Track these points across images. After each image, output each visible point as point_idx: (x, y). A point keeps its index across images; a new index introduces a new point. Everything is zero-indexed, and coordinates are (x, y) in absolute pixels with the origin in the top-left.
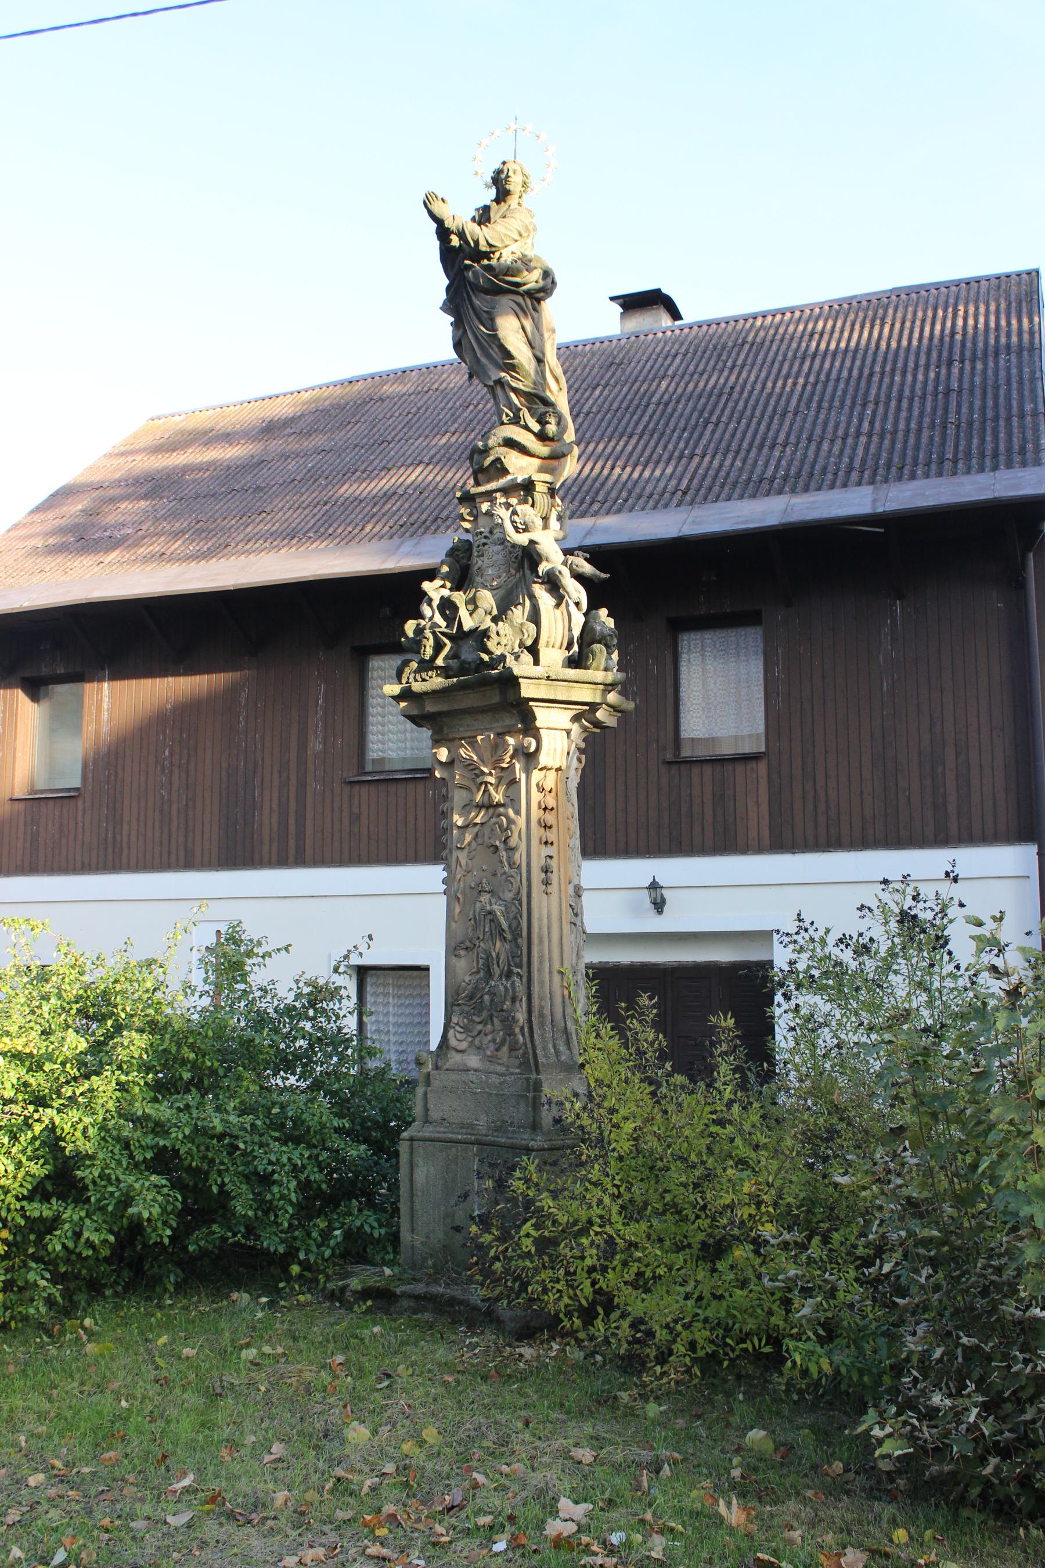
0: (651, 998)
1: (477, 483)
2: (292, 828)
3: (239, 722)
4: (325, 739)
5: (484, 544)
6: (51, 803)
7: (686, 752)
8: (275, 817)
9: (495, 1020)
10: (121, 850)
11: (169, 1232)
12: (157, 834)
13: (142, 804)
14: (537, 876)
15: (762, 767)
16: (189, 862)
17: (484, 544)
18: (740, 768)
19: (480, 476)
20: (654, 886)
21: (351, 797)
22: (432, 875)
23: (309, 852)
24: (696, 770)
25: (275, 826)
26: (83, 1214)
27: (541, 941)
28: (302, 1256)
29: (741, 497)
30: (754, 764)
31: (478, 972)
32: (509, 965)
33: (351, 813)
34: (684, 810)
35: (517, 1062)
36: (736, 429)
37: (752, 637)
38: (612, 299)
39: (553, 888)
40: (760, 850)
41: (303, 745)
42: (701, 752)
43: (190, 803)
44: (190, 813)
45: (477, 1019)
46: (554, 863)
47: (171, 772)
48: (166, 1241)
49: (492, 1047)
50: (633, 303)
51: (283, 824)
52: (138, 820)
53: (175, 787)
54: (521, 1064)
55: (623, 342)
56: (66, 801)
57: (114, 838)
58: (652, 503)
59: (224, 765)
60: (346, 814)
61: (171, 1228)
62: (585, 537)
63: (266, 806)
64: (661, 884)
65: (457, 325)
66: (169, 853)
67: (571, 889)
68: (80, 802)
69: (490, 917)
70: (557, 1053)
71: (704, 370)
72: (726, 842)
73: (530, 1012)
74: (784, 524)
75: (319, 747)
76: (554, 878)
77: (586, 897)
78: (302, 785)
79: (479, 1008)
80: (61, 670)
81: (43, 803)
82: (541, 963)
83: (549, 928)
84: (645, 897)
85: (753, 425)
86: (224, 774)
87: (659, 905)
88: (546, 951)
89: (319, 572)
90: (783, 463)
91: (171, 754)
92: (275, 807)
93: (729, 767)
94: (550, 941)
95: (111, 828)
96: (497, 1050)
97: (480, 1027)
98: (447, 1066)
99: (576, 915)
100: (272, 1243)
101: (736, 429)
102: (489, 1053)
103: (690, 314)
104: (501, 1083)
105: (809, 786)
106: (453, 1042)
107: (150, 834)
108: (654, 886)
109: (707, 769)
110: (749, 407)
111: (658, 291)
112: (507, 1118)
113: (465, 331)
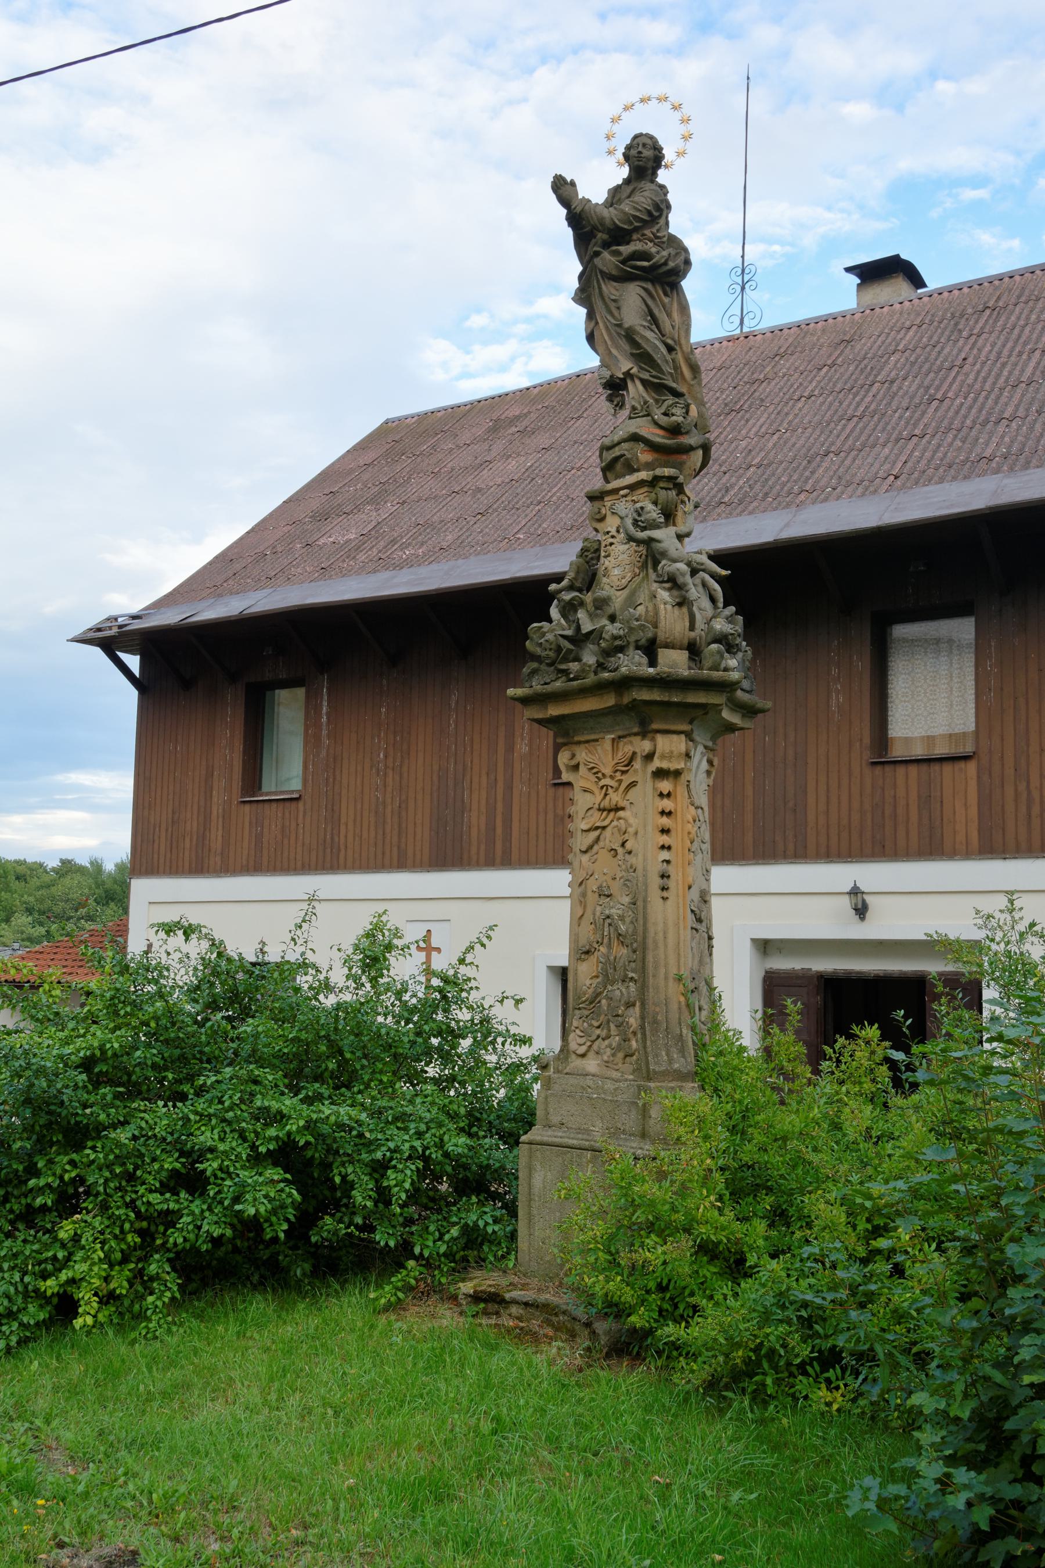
0: (795, 1003)
1: (607, 481)
2: (499, 831)
3: (449, 725)
4: (531, 740)
5: (611, 544)
6: (274, 805)
7: (898, 752)
8: (483, 818)
9: (612, 1025)
10: (339, 850)
11: (285, 1227)
12: (373, 834)
13: (359, 806)
14: (655, 882)
15: (971, 767)
16: (402, 863)
17: (611, 544)
18: (947, 768)
19: (608, 474)
20: (855, 892)
21: (555, 799)
22: (557, 880)
23: (515, 856)
24: (901, 770)
25: (483, 827)
26: (205, 1207)
27: (656, 947)
28: (417, 1250)
29: (954, 478)
30: (962, 764)
31: (597, 977)
32: (626, 970)
33: (555, 815)
34: (887, 812)
35: (631, 1068)
36: (962, 404)
37: (964, 629)
38: (848, 270)
39: (670, 894)
40: (968, 854)
41: (510, 749)
42: (919, 751)
43: (403, 806)
44: (404, 814)
45: (596, 1024)
46: (671, 869)
47: (385, 774)
48: (282, 1235)
49: (609, 1051)
50: (871, 273)
51: (491, 828)
52: (355, 821)
53: (389, 789)
54: (634, 1071)
55: (858, 316)
56: (287, 804)
57: (332, 839)
58: (860, 490)
59: (436, 768)
60: (550, 816)
61: (287, 1220)
62: (781, 530)
63: (475, 806)
64: (863, 888)
65: (591, 316)
66: (383, 853)
67: (694, 894)
68: (301, 804)
69: (608, 921)
70: (671, 1061)
71: (938, 342)
72: (933, 846)
73: (643, 1018)
74: (990, 508)
75: (525, 749)
76: (671, 883)
77: (715, 902)
78: (509, 788)
79: (595, 1013)
80: (283, 676)
81: (267, 806)
82: (656, 968)
83: (665, 933)
84: (846, 902)
85: (981, 399)
86: (435, 778)
87: (861, 911)
88: (662, 956)
89: (518, 575)
90: (1007, 439)
91: (386, 757)
92: (483, 810)
93: (936, 767)
94: (666, 946)
95: (329, 829)
96: (613, 1055)
97: (598, 1032)
98: (567, 1070)
99: (699, 920)
100: (384, 1238)
101: (962, 404)
102: (605, 1058)
103: (934, 280)
104: (616, 1089)
105: (1022, 787)
106: (573, 1046)
107: (365, 835)
108: (855, 892)
109: (913, 770)
110: (980, 379)
111: (897, 257)
112: (619, 1125)
113: (597, 323)
